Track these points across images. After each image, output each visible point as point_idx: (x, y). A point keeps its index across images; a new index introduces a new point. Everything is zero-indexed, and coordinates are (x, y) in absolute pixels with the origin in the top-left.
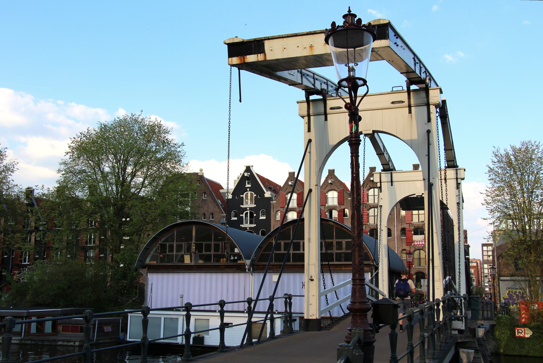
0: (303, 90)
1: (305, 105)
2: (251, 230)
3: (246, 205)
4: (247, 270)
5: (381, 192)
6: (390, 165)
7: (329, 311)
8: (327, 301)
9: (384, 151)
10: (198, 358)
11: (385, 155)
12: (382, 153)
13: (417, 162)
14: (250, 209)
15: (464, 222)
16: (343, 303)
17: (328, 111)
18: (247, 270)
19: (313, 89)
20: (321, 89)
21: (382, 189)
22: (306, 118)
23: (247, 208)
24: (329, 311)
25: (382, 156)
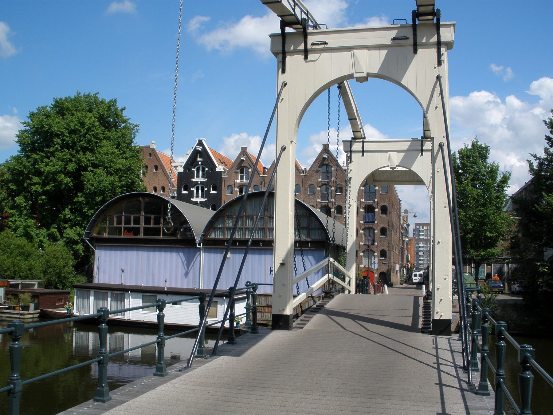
0: (279, 16)
1: (280, 39)
2: (202, 204)
3: (198, 179)
4: (197, 245)
5: (351, 162)
6: (362, 133)
7: (307, 279)
8: (304, 265)
9: (357, 116)
10: (173, 247)
11: (358, 120)
12: (355, 118)
13: (93, 400)
14: (202, 183)
15: (242, 303)
16: (310, 276)
17: (309, 47)
18: (197, 245)
19: (292, 15)
20: (301, 19)
21: (352, 160)
22: (281, 56)
23: (198, 182)
24: (307, 279)
25: (354, 121)
